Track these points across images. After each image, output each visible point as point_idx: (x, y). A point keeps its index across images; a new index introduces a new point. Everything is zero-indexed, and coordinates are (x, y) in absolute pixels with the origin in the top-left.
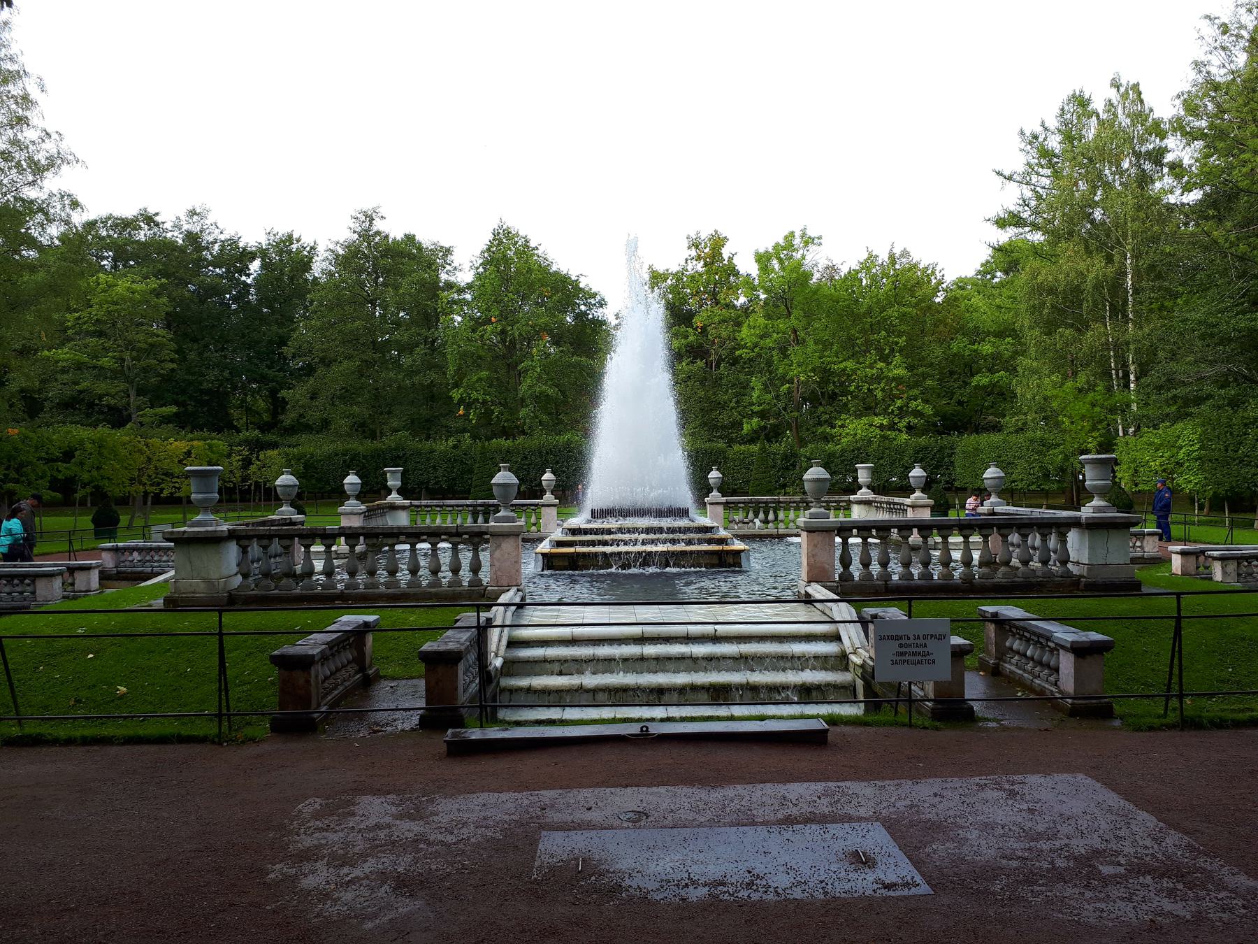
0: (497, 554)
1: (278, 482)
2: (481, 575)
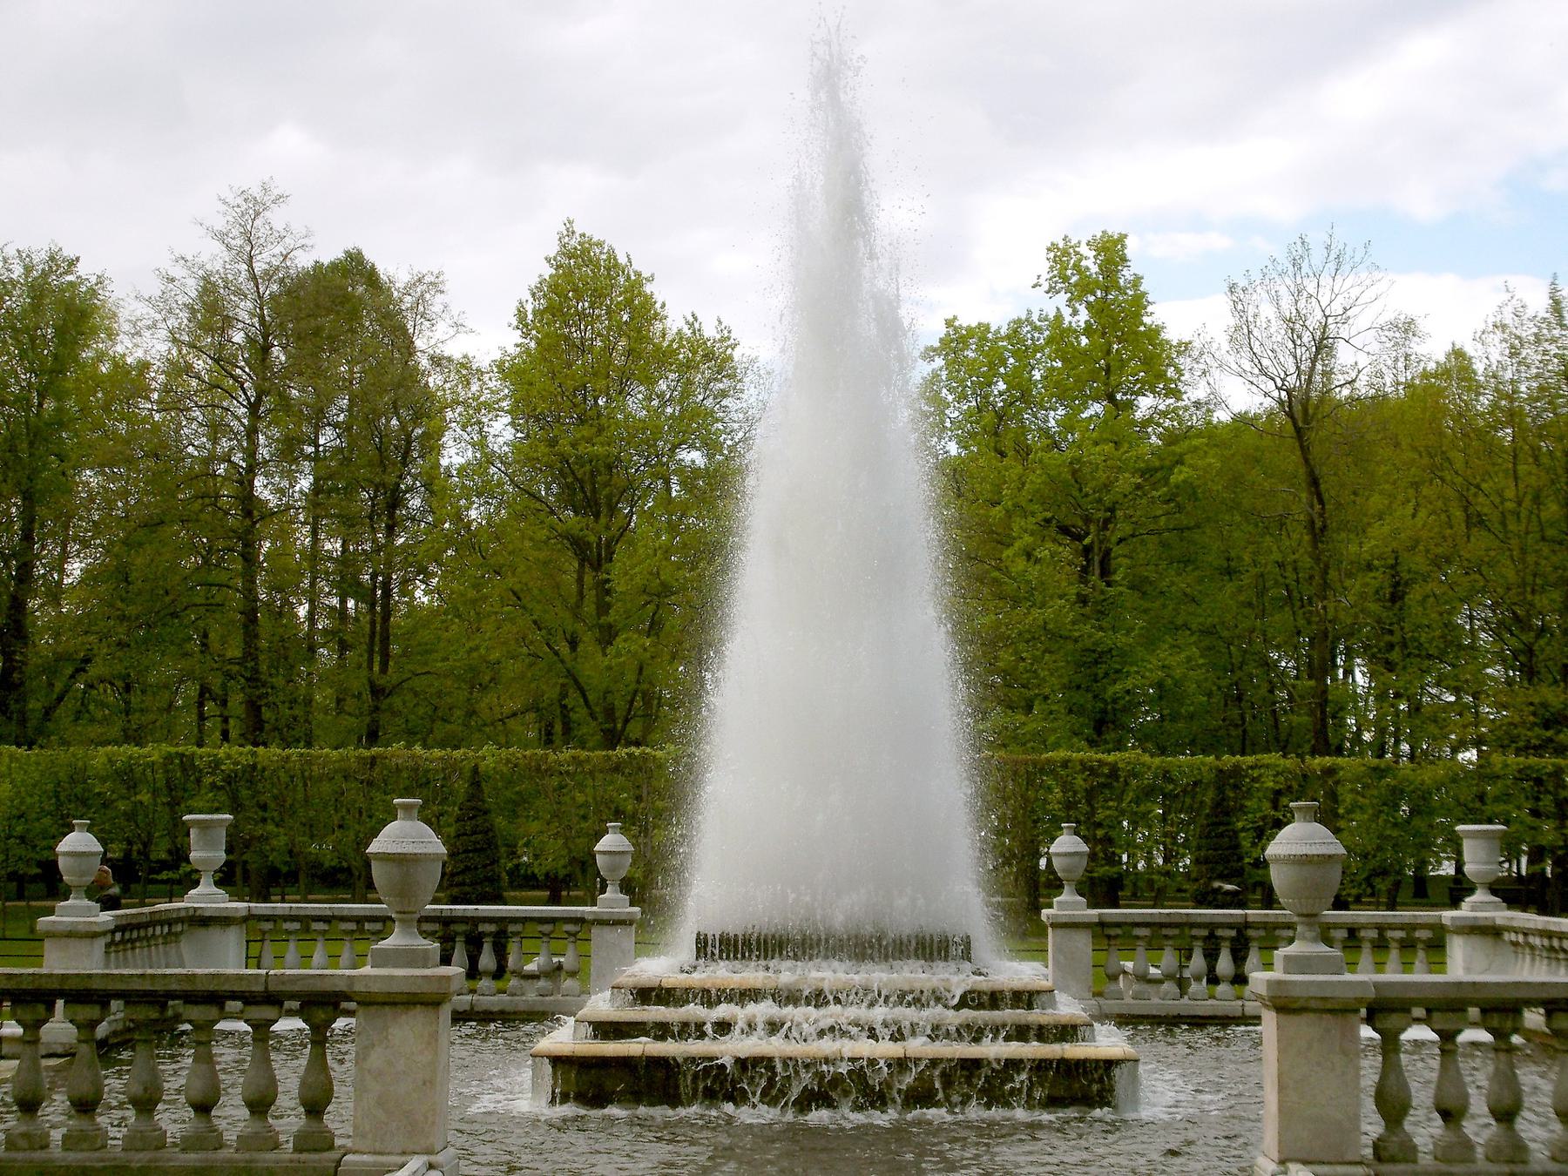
0: (376, 1059)
1: (62, 847)
2: (330, 1119)
